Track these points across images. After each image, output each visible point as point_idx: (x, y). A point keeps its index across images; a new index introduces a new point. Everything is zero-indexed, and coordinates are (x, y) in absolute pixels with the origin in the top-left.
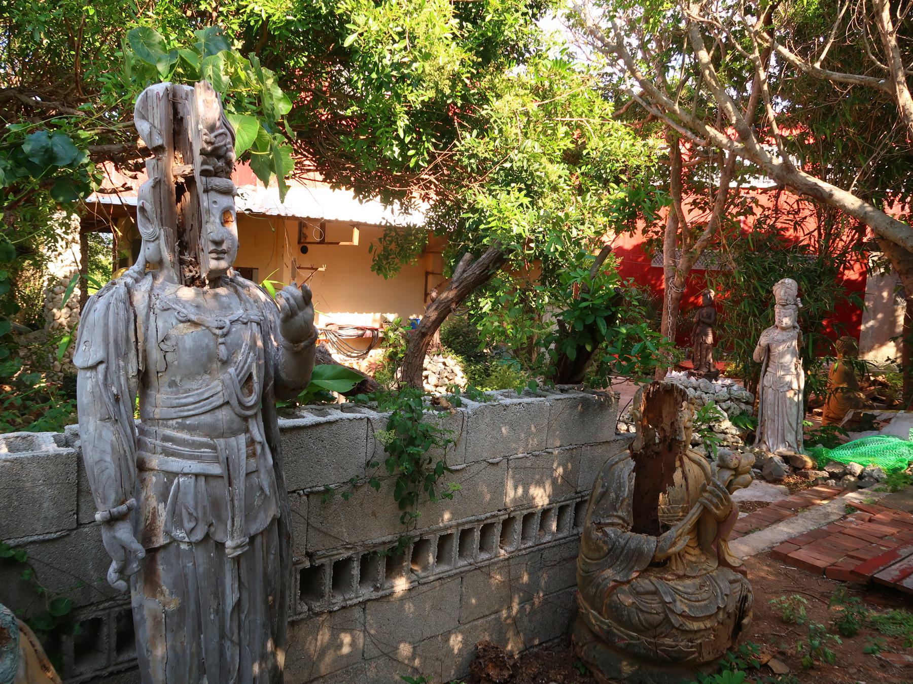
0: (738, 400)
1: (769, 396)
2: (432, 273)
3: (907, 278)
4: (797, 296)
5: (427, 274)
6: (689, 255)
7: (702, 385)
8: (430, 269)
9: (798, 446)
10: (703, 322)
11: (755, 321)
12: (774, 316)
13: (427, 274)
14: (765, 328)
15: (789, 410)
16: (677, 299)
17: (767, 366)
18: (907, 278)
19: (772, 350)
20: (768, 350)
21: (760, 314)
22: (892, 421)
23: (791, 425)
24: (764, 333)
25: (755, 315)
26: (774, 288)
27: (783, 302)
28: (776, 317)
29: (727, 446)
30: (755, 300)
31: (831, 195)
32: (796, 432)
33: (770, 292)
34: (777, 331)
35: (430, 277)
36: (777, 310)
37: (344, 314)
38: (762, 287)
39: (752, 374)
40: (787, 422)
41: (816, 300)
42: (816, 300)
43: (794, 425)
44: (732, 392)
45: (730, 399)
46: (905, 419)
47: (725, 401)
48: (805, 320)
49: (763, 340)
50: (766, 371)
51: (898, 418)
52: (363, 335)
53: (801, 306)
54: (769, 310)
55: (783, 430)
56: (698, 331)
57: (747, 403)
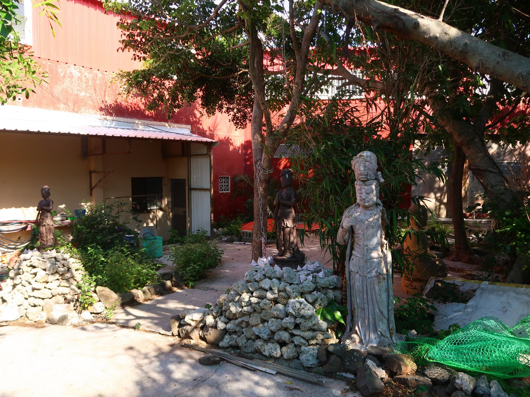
0: (323, 289)
1: (357, 282)
2: (94, 172)
3: (469, 148)
4: (378, 170)
5: (91, 172)
6: (272, 137)
7: (285, 275)
8: (93, 168)
9: (391, 334)
10: (283, 205)
11: (336, 200)
12: (355, 193)
13: (91, 172)
14: (347, 207)
15: (378, 298)
16: (265, 180)
17: (352, 249)
18: (469, 148)
19: (356, 232)
20: (352, 230)
21: (342, 191)
22: (478, 293)
23: (382, 313)
24: (346, 213)
25: (336, 193)
26: (353, 162)
27: (363, 177)
28: (358, 194)
29: (317, 344)
30: (335, 177)
31: (417, 25)
32: (388, 320)
33: (349, 168)
34: (359, 210)
35: (93, 175)
36: (357, 187)
37: (9, 210)
38: (341, 163)
39: (341, 256)
40: (378, 311)
41: (395, 174)
42: (395, 174)
43: (385, 313)
44: (318, 280)
45: (316, 289)
46: (491, 292)
47: (310, 293)
48: (386, 196)
49: (346, 222)
50: (351, 255)
51: (483, 289)
52: (25, 228)
53: (382, 180)
54: (350, 187)
55: (374, 319)
56: (279, 214)
57: (335, 289)
